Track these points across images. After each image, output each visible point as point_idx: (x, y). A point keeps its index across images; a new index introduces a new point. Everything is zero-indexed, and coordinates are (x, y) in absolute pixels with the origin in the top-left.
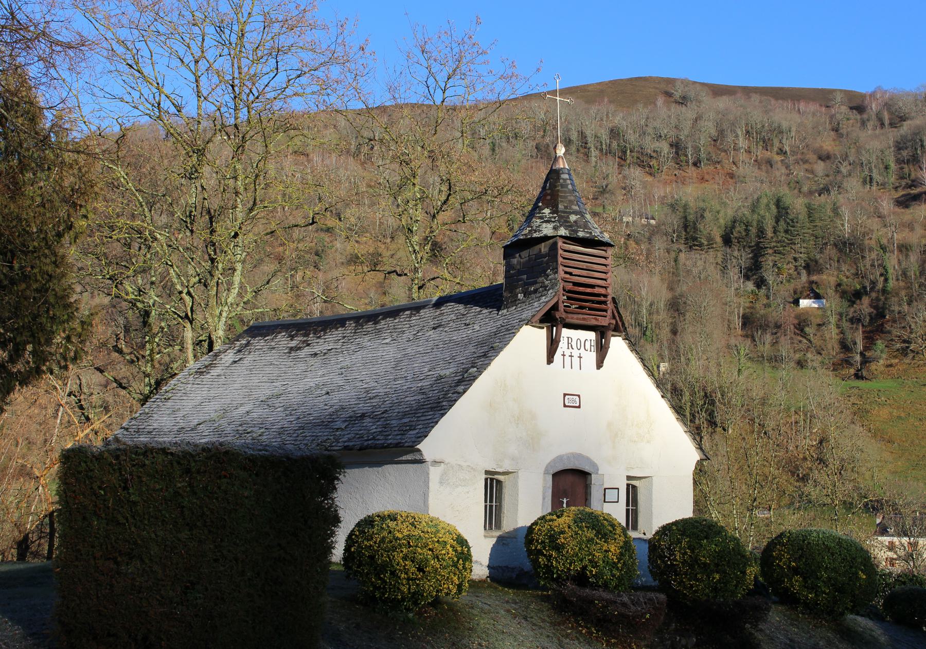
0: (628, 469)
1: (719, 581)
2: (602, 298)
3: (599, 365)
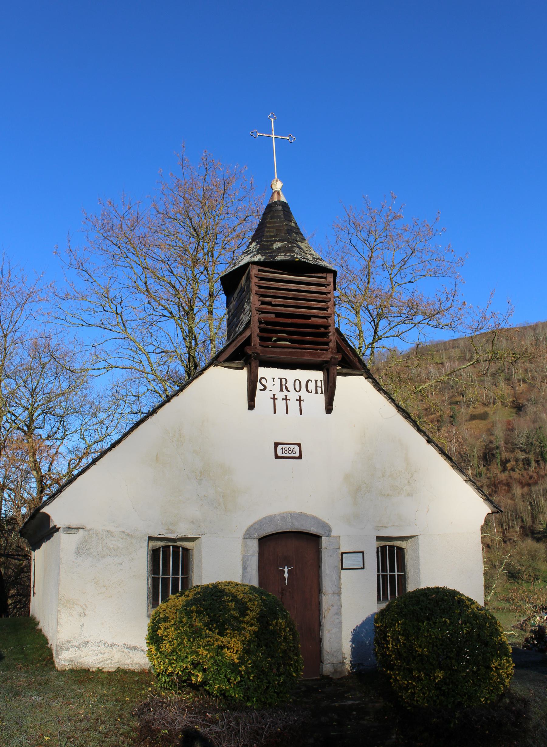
0: (377, 528)
1: (443, 681)
2: (322, 330)
3: (329, 409)
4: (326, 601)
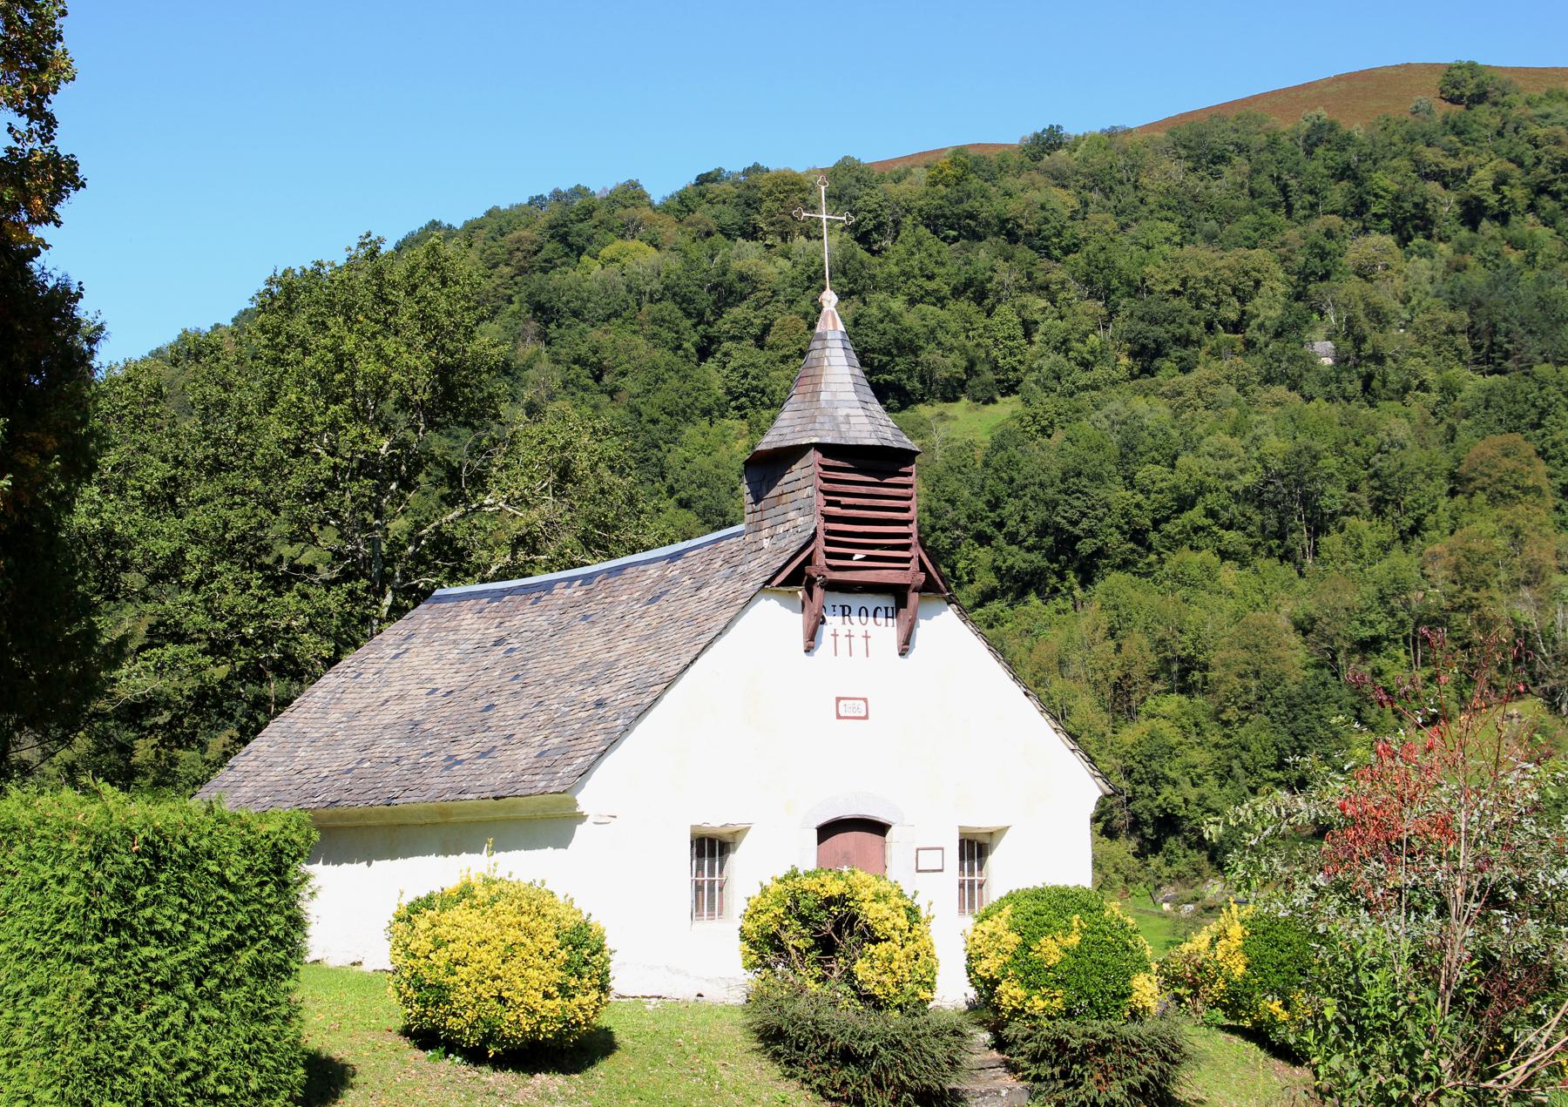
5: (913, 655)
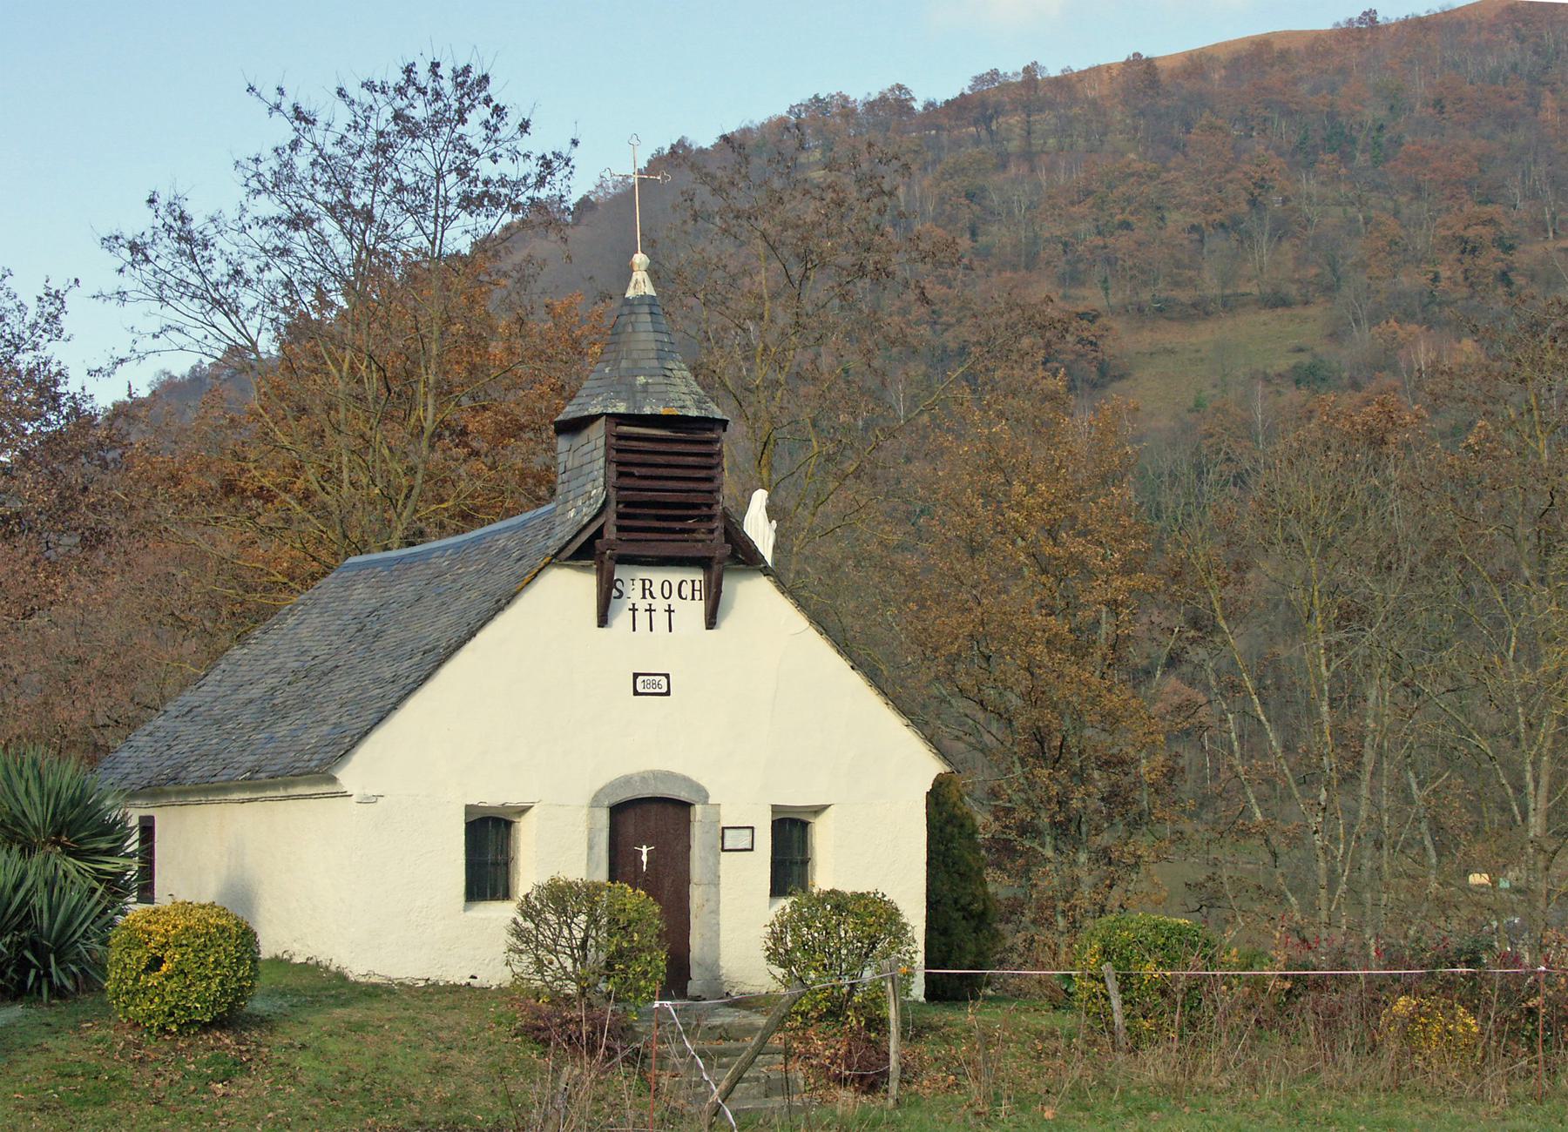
3: (711, 622)
4: (696, 895)
5: (727, 624)
